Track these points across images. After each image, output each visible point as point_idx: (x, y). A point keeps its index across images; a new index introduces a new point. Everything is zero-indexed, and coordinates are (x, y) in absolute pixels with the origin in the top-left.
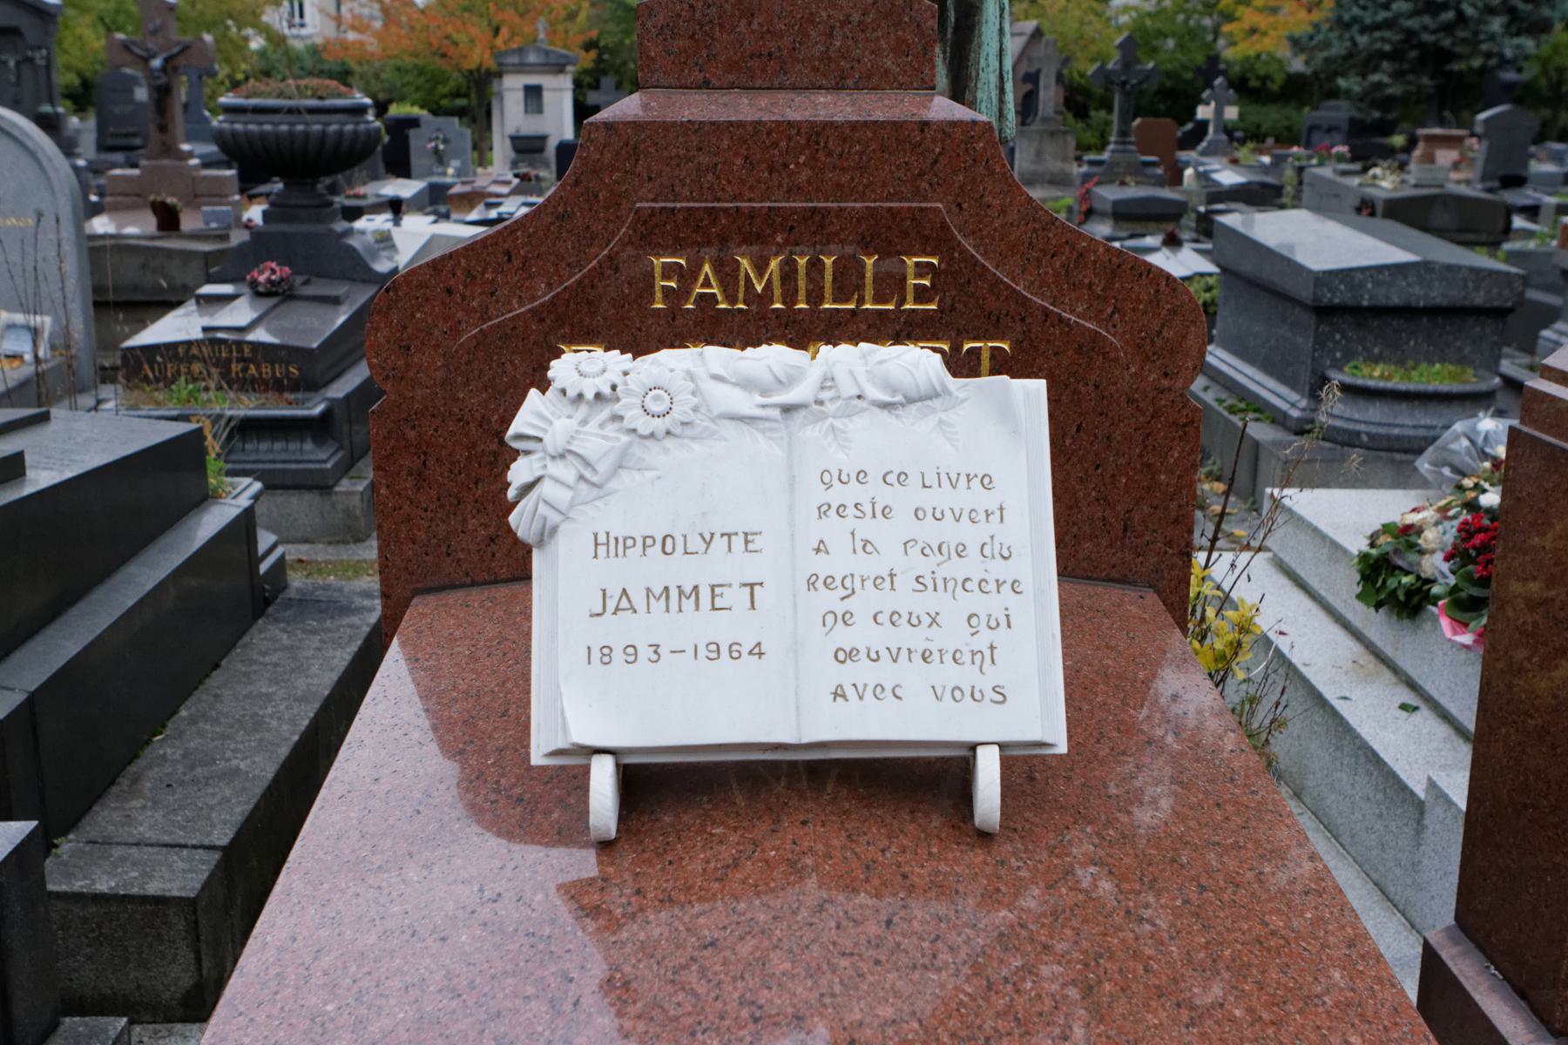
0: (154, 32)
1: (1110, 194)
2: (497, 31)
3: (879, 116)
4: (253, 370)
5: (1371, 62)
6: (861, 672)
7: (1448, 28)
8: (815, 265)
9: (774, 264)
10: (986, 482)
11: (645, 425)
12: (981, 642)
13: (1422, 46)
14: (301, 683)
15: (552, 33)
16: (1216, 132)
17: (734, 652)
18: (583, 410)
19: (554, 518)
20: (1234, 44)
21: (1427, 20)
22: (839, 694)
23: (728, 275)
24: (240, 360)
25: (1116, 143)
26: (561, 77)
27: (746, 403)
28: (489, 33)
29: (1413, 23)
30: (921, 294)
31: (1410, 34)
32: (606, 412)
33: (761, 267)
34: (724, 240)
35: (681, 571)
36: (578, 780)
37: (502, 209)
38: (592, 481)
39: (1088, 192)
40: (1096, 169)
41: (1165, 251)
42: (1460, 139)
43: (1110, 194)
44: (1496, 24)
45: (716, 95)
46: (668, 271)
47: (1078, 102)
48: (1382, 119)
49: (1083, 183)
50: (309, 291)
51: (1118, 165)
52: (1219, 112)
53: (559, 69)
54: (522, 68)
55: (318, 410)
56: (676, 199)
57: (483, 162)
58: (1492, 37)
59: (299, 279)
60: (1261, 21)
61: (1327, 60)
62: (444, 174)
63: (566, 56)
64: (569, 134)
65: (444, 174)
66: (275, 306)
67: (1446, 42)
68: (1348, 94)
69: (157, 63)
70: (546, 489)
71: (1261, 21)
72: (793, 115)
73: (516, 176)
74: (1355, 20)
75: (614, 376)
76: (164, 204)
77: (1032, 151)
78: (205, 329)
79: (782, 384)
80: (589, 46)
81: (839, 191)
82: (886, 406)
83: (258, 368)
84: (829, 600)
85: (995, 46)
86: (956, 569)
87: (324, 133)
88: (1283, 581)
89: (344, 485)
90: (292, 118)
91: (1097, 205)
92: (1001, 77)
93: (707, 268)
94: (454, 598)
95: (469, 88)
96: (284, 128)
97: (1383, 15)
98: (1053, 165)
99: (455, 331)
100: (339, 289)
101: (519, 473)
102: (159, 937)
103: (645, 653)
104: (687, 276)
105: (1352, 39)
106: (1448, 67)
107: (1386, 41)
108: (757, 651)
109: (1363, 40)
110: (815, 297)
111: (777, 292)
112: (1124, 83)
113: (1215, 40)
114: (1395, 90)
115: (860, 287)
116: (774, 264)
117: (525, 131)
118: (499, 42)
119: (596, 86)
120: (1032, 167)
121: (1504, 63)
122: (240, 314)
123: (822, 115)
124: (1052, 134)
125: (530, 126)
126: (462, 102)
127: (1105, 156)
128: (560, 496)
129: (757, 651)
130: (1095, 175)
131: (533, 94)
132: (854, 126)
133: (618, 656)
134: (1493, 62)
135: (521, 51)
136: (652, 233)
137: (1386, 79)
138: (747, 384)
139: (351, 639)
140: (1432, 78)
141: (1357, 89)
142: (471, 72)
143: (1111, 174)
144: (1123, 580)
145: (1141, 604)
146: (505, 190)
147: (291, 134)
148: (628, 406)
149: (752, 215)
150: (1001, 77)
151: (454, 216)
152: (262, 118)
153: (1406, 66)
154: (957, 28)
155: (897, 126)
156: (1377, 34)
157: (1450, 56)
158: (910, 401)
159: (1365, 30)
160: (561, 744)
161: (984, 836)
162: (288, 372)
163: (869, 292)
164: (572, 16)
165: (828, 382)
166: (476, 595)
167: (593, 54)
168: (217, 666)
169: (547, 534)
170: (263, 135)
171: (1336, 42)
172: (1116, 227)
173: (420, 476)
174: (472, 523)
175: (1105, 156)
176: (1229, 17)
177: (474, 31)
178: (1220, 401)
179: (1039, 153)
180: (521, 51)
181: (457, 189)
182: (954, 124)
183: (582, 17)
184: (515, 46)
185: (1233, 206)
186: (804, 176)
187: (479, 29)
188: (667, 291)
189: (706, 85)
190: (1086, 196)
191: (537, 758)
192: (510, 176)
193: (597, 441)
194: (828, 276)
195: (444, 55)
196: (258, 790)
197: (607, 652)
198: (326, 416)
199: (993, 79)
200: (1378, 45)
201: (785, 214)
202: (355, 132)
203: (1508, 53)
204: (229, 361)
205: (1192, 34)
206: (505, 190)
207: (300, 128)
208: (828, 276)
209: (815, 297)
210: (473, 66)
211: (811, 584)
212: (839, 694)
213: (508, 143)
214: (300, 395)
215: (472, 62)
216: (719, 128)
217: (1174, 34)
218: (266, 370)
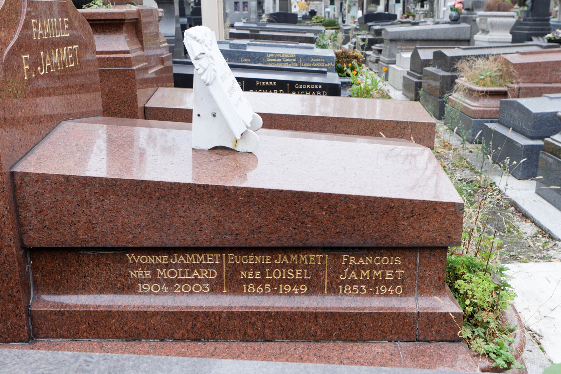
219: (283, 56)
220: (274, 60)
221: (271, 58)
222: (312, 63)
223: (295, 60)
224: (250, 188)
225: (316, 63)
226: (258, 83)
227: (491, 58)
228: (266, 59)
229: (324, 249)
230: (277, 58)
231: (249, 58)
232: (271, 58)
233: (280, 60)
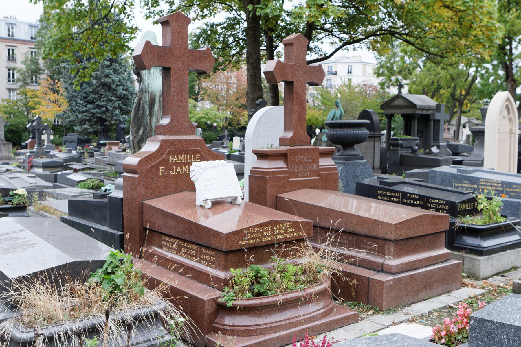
5: (82, 122)
7: (104, 113)
8: (187, 156)
13: (97, 117)
16: (48, 142)
21: (98, 110)
23: (178, 158)
29: (94, 111)
31: (93, 114)
39: (31, 160)
40: (32, 154)
41: (74, 173)
42: (118, 143)
44: (117, 112)
48: (88, 138)
49: (29, 158)
51: (39, 152)
58: (117, 115)
61: (69, 121)
67: (104, 117)
68: (77, 131)
74: (77, 110)
81: (189, 147)
97: (85, 109)
104: (173, 158)
105: (77, 115)
106: (105, 124)
107: (87, 116)
109: (80, 116)
110: (187, 160)
112: (39, 129)
113: (28, 114)
114: (91, 130)
121: (121, 122)
134: (117, 122)
136: (169, 153)
137: (88, 127)
140: (101, 126)
141: (80, 130)
153: (93, 123)
156: (84, 114)
157: (105, 120)
159: (80, 112)
171: (71, 116)
185: (73, 163)
193: (196, 169)
200: (85, 117)
203: (122, 120)
209: (187, 160)
216: (176, 140)
219: (492, 181)
220: (485, 184)
221: (483, 182)
222: (513, 188)
223: (500, 185)
224: (400, 264)
225: (516, 188)
226: (408, 195)
227: (22, 167)
228: (480, 182)
229: (198, 244)
230: (488, 182)
231: (468, 181)
232: (483, 182)
233: (489, 184)
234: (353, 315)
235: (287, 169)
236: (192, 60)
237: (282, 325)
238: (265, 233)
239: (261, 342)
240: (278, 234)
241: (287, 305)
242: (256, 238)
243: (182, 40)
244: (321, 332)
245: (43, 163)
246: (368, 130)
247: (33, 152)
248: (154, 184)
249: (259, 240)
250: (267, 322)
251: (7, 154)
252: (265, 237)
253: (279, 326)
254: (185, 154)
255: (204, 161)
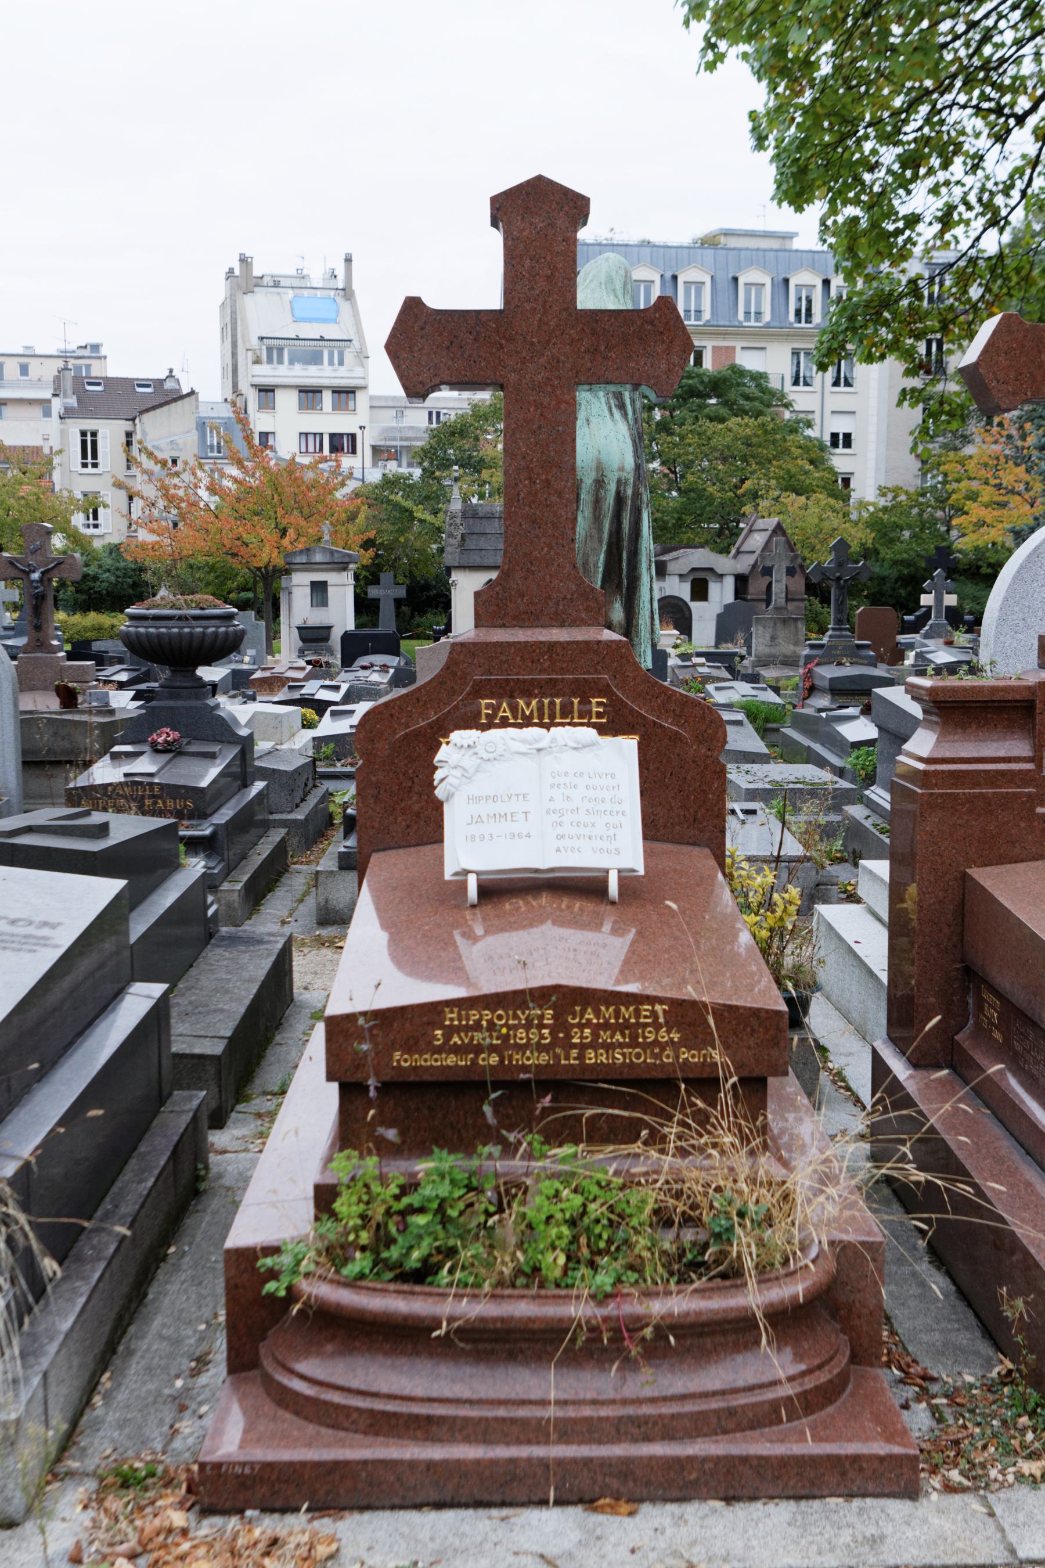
0: (34, 552)
1: (828, 672)
2: (284, 532)
3: (579, 638)
4: (160, 804)
6: (565, 843)
8: (552, 704)
9: (534, 702)
10: (613, 776)
11: (486, 756)
12: (611, 833)
14: (246, 975)
15: (334, 534)
17: (520, 836)
18: (463, 751)
19: (453, 790)
20: (963, 535)
22: (558, 850)
24: (151, 797)
25: (833, 629)
26: (345, 574)
27: (523, 748)
28: (276, 535)
30: (599, 715)
32: (471, 751)
33: (528, 705)
34: (512, 697)
35: (500, 808)
36: (463, 886)
37: (303, 691)
38: (467, 776)
39: (810, 671)
40: (815, 652)
41: (862, 718)
43: (828, 672)
45: (508, 630)
46: (488, 706)
47: (816, 590)
50: (193, 748)
51: (836, 648)
52: (939, 600)
53: (343, 567)
54: (309, 566)
55: (207, 832)
56: (491, 674)
57: (270, 651)
59: (185, 741)
60: (988, 515)
62: (242, 662)
63: (349, 555)
64: (351, 626)
65: (242, 662)
66: (168, 763)
69: (36, 576)
70: (450, 780)
71: (988, 515)
72: (542, 639)
73: (309, 663)
75: (474, 738)
76: (66, 687)
77: (768, 637)
78: (126, 775)
79: (536, 741)
80: (367, 544)
81: (563, 671)
82: (575, 749)
83: (164, 803)
84: (555, 817)
85: (648, 597)
86: (601, 807)
87: (204, 633)
88: (870, 917)
89: (225, 886)
90: (181, 623)
91: (818, 683)
92: (652, 612)
93: (505, 705)
94: (392, 853)
95: (255, 582)
96: (175, 630)
98: (787, 648)
99: (395, 733)
100: (215, 748)
101: (438, 775)
102: (200, 1078)
103: (487, 837)
104: (496, 709)
108: (528, 836)
111: (536, 714)
112: (839, 579)
113: (948, 531)
115: (572, 712)
116: (534, 702)
117: (311, 623)
118: (286, 542)
119: (376, 581)
120: (767, 650)
122: (145, 765)
123: (554, 638)
124: (784, 621)
125: (316, 618)
126: (245, 595)
127: (825, 640)
128: (456, 782)
129: (528, 836)
130: (815, 656)
131: (319, 589)
132: (568, 643)
133: (477, 839)
135: (308, 551)
138: (524, 741)
139: (269, 955)
142: (259, 569)
143: (830, 657)
144: (695, 844)
145: (701, 858)
146: (300, 675)
147: (180, 634)
148: (480, 750)
149: (524, 681)
150: (652, 612)
151: (259, 698)
152: (158, 623)
154: (628, 588)
155: (587, 643)
158: (584, 747)
160: (458, 869)
161: (613, 903)
162: (186, 805)
163: (576, 714)
164: (352, 517)
165: (554, 740)
166: (401, 851)
167: (371, 552)
168: (191, 966)
169: (450, 796)
170: (159, 636)
172: (832, 701)
173: (376, 797)
174: (399, 819)
175: (825, 640)
176: (961, 511)
177: (263, 533)
178: (875, 825)
179: (773, 638)
180: (308, 551)
181: (258, 675)
182: (612, 642)
183: (361, 518)
184: (300, 546)
186: (546, 665)
187: (267, 532)
188: (487, 715)
189: (503, 626)
190: (809, 675)
191: (447, 877)
192: (303, 664)
193: (469, 762)
194: (558, 707)
195: (234, 555)
196: (238, 1017)
197: (473, 838)
198: (214, 834)
199: (647, 613)
201: (539, 681)
202: (226, 633)
204: (143, 797)
205: (925, 524)
206: (300, 675)
207: (187, 630)
208: (558, 707)
210: (261, 564)
211: (548, 812)
212: (558, 850)
213: (295, 632)
214: (194, 822)
215: (260, 562)
217: (909, 527)
218: (170, 804)
234: (881, 1459)
235: (1030, 766)
236: (594, 351)
237: (466, 1420)
238: (521, 1033)
239: (347, 1463)
240: (594, 1045)
241: (525, 1346)
242: (478, 1049)
243: (549, 278)
244: (675, 1493)
245: (831, 679)
246: (675, 628)
247: (822, 646)
248: (420, 794)
249: (494, 1060)
250: (407, 1392)
251: (792, 647)
252: (521, 1048)
253: (454, 1419)
254: (543, 695)
255: (470, 728)
